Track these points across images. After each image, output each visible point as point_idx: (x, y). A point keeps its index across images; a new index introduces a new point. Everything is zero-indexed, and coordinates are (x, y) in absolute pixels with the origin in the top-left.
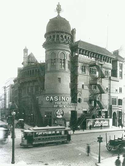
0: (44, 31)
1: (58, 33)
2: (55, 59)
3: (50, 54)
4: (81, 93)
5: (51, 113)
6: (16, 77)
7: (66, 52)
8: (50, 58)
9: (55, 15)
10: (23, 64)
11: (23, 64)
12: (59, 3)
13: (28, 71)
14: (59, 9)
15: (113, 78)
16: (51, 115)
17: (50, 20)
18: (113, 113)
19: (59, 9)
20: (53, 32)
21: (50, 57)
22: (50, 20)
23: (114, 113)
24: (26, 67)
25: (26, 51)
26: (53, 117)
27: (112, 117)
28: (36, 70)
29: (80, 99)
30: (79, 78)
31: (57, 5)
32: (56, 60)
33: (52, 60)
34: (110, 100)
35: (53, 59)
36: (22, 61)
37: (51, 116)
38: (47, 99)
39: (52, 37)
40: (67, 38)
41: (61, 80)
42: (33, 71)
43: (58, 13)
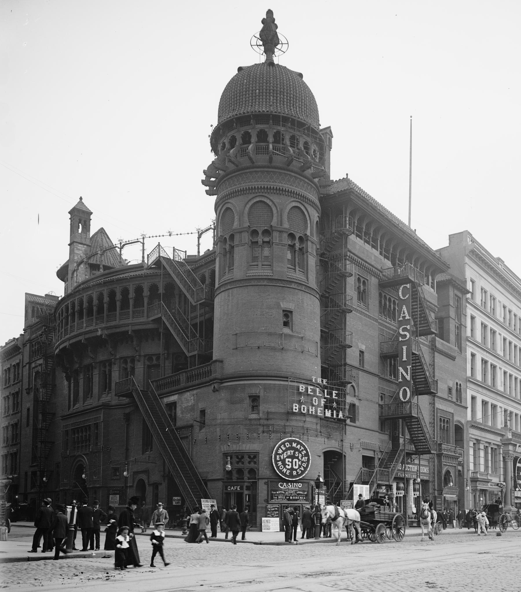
1: (265, 129)
2: (267, 232)
3: (247, 209)
4: (358, 386)
5: (254, 456)
6: (17, 336)
8: (247, 224)
9: (256, 57)
10: (63, 274)
11: (63, 274)
12: (270, 13)
13: (112, 295)
14: (269, 37)
15: (442, 344)
16: (252, 465)
17: (240, 69)
18: (444, 472)
19: (269, 37)
21: (246, 219)
22: (240, 69)
23: (397, 517)
25: (80, 216)
26: (264, 471)
29: (353, 406)
30: (353, 322)
31: (263, 21)
32: (275, 234)
33: (255, 233)
34: (434, 423)
36: (63, 256)
38: (404, 296)
41: (296, 317)
43: (265, 52)
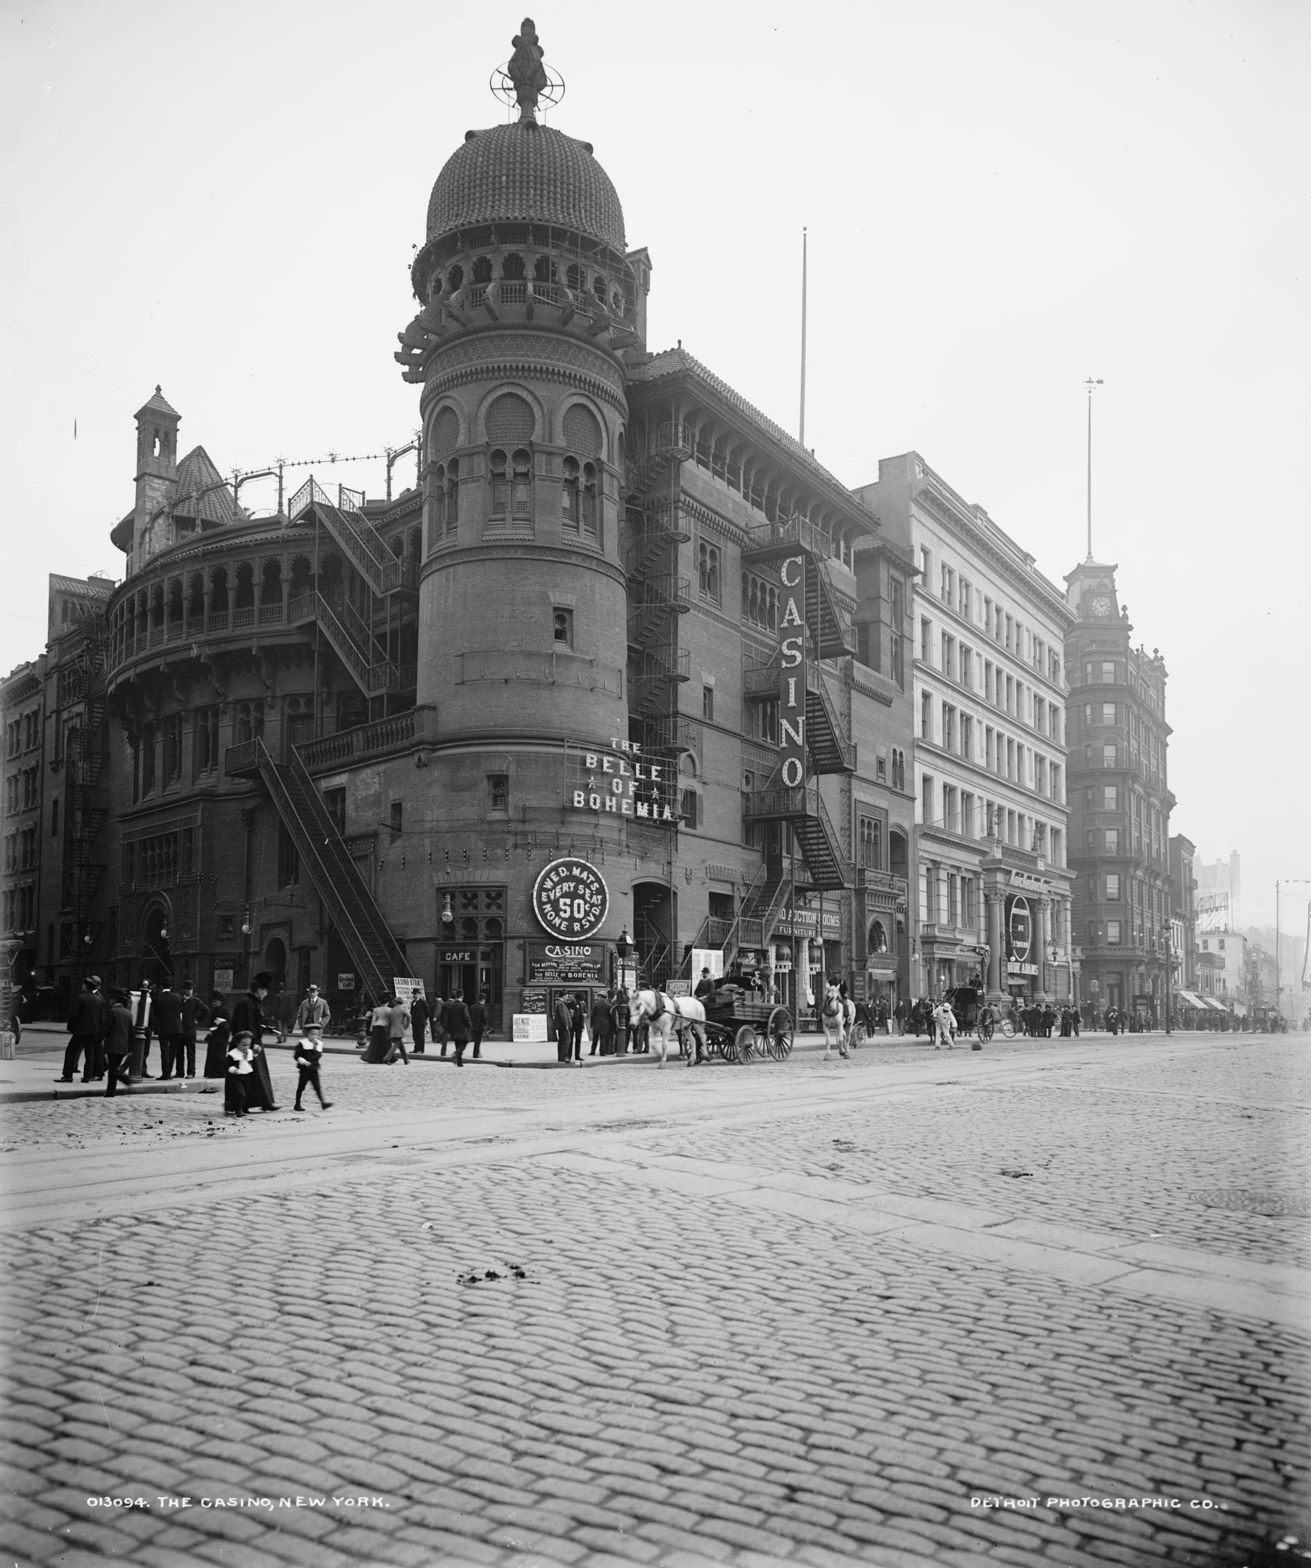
0: (413, 233)
1: (519, 252)
2: (522, 455)
3: (483, 409)
5: (497, 895)
6: (34, 658)
7: (542, 390)
8: (483, 440)
9: (501, 111)
11: (123, 536)
14: (527, 71)
16: (494, 911)
17: (470, 135)
19: (527, 71)
20: (475, 235)
21: (482, 428)
22: (470, 135)
24: (859, 508)
26: (516, 923)
27: (579, 753)
28: (301, 565)
33: (499, 456)
35: (509, 456)
36: (123, 503)
37: (494, 924)
39: (468, 276)
40: (590, 285)
42: (272, 569)
